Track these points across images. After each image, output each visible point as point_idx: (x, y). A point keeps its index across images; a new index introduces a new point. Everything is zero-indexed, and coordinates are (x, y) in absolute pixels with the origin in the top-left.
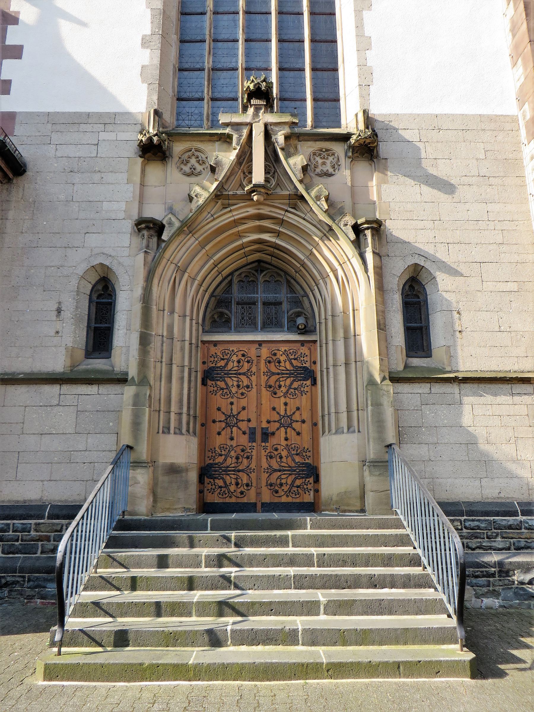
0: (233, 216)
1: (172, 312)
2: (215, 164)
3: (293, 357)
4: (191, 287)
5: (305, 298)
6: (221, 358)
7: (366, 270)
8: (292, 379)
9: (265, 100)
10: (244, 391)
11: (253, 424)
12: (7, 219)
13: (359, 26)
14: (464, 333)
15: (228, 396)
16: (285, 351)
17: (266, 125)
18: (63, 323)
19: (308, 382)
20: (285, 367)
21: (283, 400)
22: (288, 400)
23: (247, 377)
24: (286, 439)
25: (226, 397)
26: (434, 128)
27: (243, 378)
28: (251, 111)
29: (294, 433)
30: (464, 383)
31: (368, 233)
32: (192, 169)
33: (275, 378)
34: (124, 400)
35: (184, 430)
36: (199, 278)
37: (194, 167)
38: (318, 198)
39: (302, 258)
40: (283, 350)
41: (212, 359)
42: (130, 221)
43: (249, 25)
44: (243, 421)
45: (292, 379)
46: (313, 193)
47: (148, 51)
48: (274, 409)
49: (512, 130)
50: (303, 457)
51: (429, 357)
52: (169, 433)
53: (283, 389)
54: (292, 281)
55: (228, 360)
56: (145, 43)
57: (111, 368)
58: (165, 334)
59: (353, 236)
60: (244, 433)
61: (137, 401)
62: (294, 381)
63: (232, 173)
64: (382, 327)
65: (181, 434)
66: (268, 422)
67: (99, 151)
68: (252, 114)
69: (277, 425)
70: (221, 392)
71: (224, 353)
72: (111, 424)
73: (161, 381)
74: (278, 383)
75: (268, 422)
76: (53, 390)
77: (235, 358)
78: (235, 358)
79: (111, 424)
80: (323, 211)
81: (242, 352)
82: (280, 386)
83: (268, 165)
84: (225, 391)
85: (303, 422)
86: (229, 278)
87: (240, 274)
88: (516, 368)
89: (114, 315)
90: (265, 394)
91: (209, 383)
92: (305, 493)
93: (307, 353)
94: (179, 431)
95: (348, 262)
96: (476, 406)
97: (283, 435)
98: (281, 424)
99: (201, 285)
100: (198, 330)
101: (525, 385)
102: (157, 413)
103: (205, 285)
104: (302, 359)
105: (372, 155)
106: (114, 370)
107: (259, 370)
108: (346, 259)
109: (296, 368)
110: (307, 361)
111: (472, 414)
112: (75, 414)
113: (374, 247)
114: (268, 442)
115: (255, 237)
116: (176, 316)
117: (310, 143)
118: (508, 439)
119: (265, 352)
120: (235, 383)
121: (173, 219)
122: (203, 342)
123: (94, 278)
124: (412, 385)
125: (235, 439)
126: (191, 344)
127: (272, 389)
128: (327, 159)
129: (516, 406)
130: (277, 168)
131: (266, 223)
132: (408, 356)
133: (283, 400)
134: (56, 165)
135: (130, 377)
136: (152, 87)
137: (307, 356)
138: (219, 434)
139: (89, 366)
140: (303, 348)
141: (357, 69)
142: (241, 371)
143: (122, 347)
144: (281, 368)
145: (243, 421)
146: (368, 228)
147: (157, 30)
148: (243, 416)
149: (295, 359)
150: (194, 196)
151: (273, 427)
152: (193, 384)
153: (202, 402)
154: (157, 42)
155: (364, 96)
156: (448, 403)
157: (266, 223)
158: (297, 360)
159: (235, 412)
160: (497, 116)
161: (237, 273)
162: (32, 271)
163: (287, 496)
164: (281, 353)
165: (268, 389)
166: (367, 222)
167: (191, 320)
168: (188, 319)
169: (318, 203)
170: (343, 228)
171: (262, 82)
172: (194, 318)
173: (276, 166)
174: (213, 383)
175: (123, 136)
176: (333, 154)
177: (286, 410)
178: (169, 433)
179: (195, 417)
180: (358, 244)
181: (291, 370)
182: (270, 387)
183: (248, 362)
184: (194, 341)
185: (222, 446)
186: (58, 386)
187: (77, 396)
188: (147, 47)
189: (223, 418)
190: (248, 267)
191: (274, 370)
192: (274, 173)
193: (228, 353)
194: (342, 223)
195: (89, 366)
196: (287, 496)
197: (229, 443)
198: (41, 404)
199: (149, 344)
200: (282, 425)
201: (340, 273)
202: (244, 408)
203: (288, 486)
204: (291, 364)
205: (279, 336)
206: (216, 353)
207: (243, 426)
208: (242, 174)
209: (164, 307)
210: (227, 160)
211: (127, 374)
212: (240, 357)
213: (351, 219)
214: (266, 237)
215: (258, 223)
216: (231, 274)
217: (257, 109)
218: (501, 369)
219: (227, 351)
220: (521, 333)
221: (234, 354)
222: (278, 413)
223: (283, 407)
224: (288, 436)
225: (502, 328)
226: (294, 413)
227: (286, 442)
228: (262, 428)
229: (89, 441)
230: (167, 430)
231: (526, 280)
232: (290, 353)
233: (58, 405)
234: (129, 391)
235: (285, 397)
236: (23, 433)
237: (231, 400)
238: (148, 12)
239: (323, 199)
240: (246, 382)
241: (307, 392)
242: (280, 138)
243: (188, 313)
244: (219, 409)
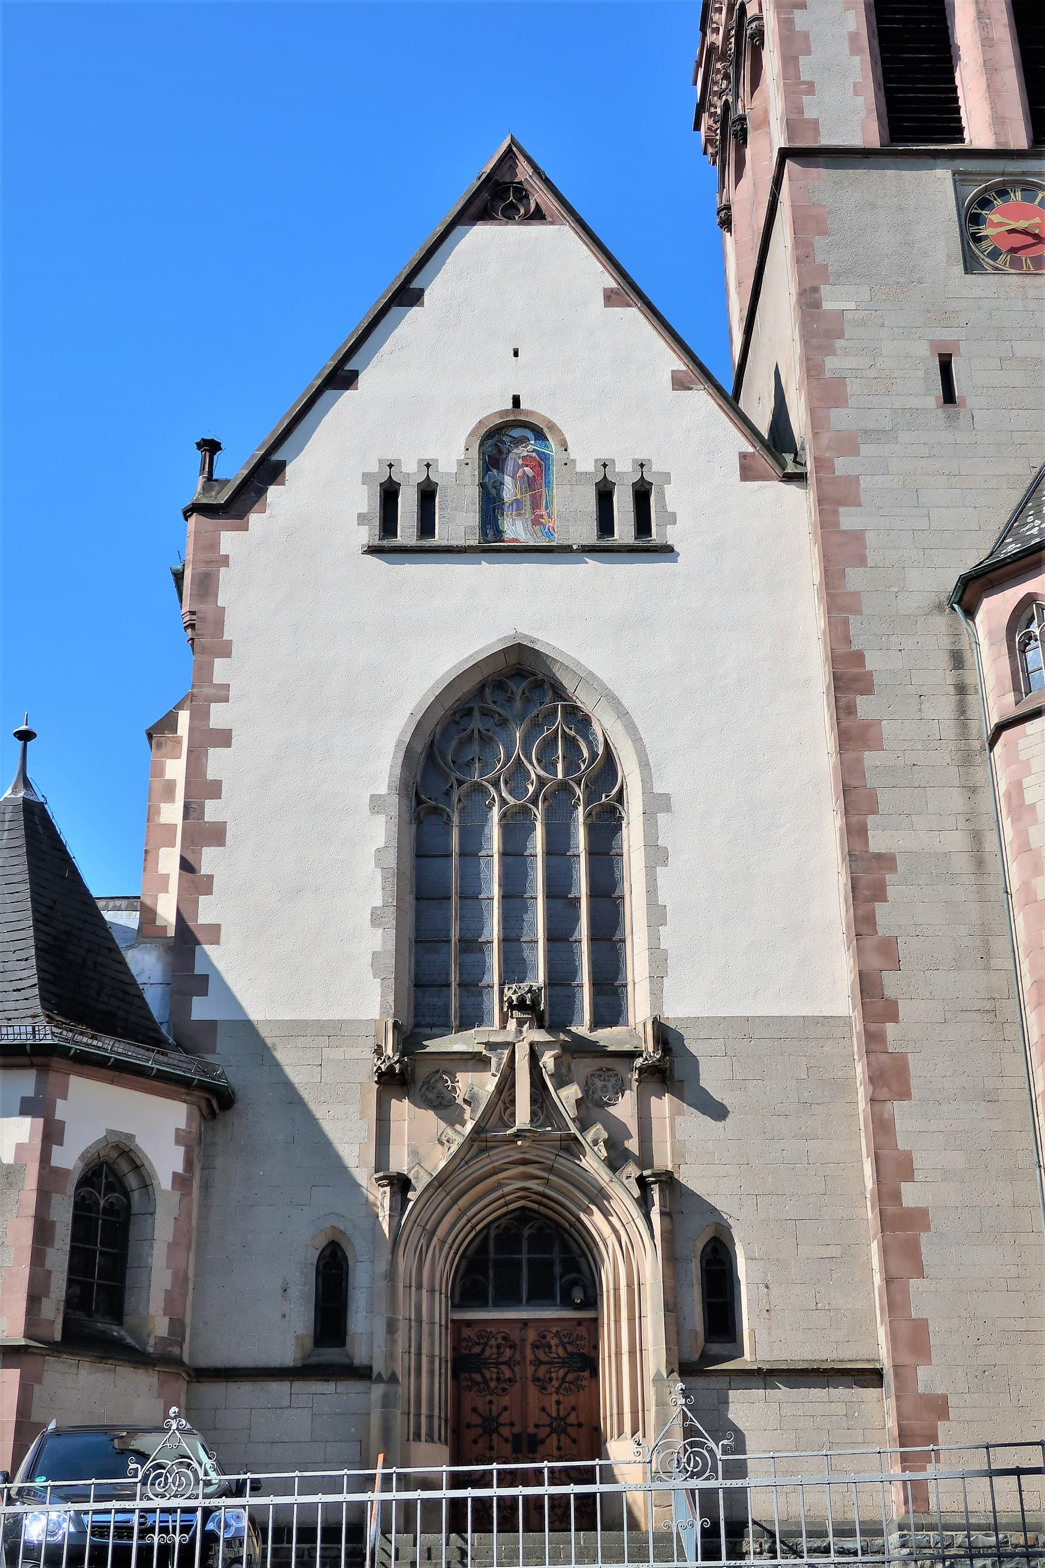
0: (492, 1162)
1: (419, 1287)
2: (471, 1098)
3: (566, 1340)
5: (583, 1260)
6: (476, 1343)
7: (653, 1237)
8: (566, 1369)
9: (530, 1012)
10: (506, 1386)
11: (516, 1430)
12: (214, 1168)
13: (652, 890)
14: (772, 1313)
15: (486, 1393)
17: (532, 1045)
18: (290, 1304)
19: (586, 1374)
20: (558, 1355)
21: (555, 1397)
22: (561, 1398)
23: (510, 1368)
25: (483, 1394)
26: (744, 1037)
27: (504, 1368)
29: (568, 1441)
30: (770, 1376)
31: (656, 1188)
32: (440, 1098)
34: (373, 1400)
36: (450, 1241)
37: (442, 1095)
40: (554, 1331)
41: (465, 1344)
42: (365, 1170)
43: (507, 917)
45: (566, 1369)
47: (380, 931)
48: (543, 1409)
49: (844, 1038)
50: (471, 1379)
51: (732, 1342)
52: (420, 1440)
53: (555, 1383)
54: (566, 1235)
55: (486, 1345)
57: (347, 1360)
58: (413, 1317)
59: (636, 1192)
60: (506, 1441)
61: (387, 1402)
62: (568, 1372)
63: (491, 1106)
64: (671, 1308)
65: (433, 1441)
66: (537, 1426)
67: (324, 1074)
68: (513, 1029)
69: (548, 1430)
70: (477, 1387)
71: (479, 1337)
72: (353, 1429)
73: (409, 1377)
74: (548, 1376)
75: (537, 1426)
76: (280, 1389)
77: (493, 1342)
79: (353, 1429)
81: (503, 1334)
82: (551, 1379)
83: (535, 1092)
84: (482, 1386)
85: (580, 1425)
86: (484, 1233)
87: (498, 1227)
88: (834, 1356)
90: (532, 1390)
91: (463, 1375)
92: (583, 1517)
93: (584, 1333)
94: (430, 1438)
95: (632, 1222)
96: (784, 1404)
97: (555, 1443)
98: (552, 1429)
99: (451, 1248)
100: (447, 1306)
101: (845, 1377)
102: (407, 1416)
103: (455, 1247)
104: (578, 1342)
105: (664, 1077)
106: (353, 1363)
107: (524, 1358)
108: (631, 1219)
109: (571, 1355)
110: (584, 1346)
111: (778, 1414)
112: (310, 1418)
113: (662, 1205)
114: (536, 1452)
116: (424, 1291)
119: (531, 1335)
120: (494, 1376)
121: (422, 1173)
122: (453, 1321)
123: (322, 1243)
124: (707, 1379)
125: (496, 1448)
126: (440, 1326)
127: (540, 1383)
128: (609, 1081)
129: (832, 1404)
130: (545, 1098)
132: (708, 1340)
133: (555, 1397)
134: (271, 1094)
136: (386, 982)
137: (585, 1338)
138: (475, 1442)
139: (321, 1358)
140: (579, 1328)
142: (501, 1360)
143: (362, 1334)
144: (553, 1355)
146: (655, 1183)
147: (390, 900)
148: (505, 1418)
149: (569, 1343)
150: (445, 1142)
151: (543, 1432)
153: (453, 1399)
154: (391, 920)
155: (656, 994)
156: (751, 1401)
158: (572, 1344)
160: (825, 1017)
162: (249, 1237)
163: (491, 1332)
164: (552, 1335)
165: (536, 1383)
166: (654, 1175)
167: (441, 1294)
168: (437, 1294)
169: (596, 1148)
170: (626, 1182)
171: (527, 993)
172: (443, 1292)
173: (543, 1095)
174: (467, 1375)
175: (354, 1053)
176: (616, 1075)
177: (558, 1411)
178: (420, 1440)
179: (446, 1421)
180: (644, 1203)
181: (564, 1358)
182: (538, 1380)
183: (510, 1347)
184: (443, 1323)
185: (479, 1458)
186: (288, 1384)
187: (311, 1396)
188: (379, 926)
190: (510, 1216)
191: (543, 1357)
192: (542, 1103)
193: (485, 1336)
194: (624, 1176)
195: (321, 1358)
196: (491, 1332)
197: (561, 1398)
198: (269, 1406)
199: (396, 1333)
200: (553, 1431)
202: (505, 1409)
203: (562, 1510)
204: (565, 1349)
205: (549, 1313)
206: (469, 1336)
207: (506, 1432)
208: (502, 1105)
209: (410, 1282)
210: (484, 1092)
212: (500, 1340)
213: (636, 1170)
215: (521, 1169)
216: (487, 1227)
217: (521, 1023)
218: (816, 1358)
219: (483, 1334)
220: (842, 1312)
221: (493, 1337)
222: (548, 1415)
223: (554, 1407)
224: (562, 1444)
225: (820, 1305)
226: (569, 1414)
227: (559, 1453)
228: (530, 1435)
229: (327, 1450)
230: (418, 1437)
232: (564, 1335)
233: (290, 1407)
234: (377, 1391)
235: (557, 1393)
236: (250, 1442)
237: (489, 1398)
239: (602, 1143)
240: (508, 1374)
241: (585, 1386)
242: (548, 1060)
243: (437, 1288)
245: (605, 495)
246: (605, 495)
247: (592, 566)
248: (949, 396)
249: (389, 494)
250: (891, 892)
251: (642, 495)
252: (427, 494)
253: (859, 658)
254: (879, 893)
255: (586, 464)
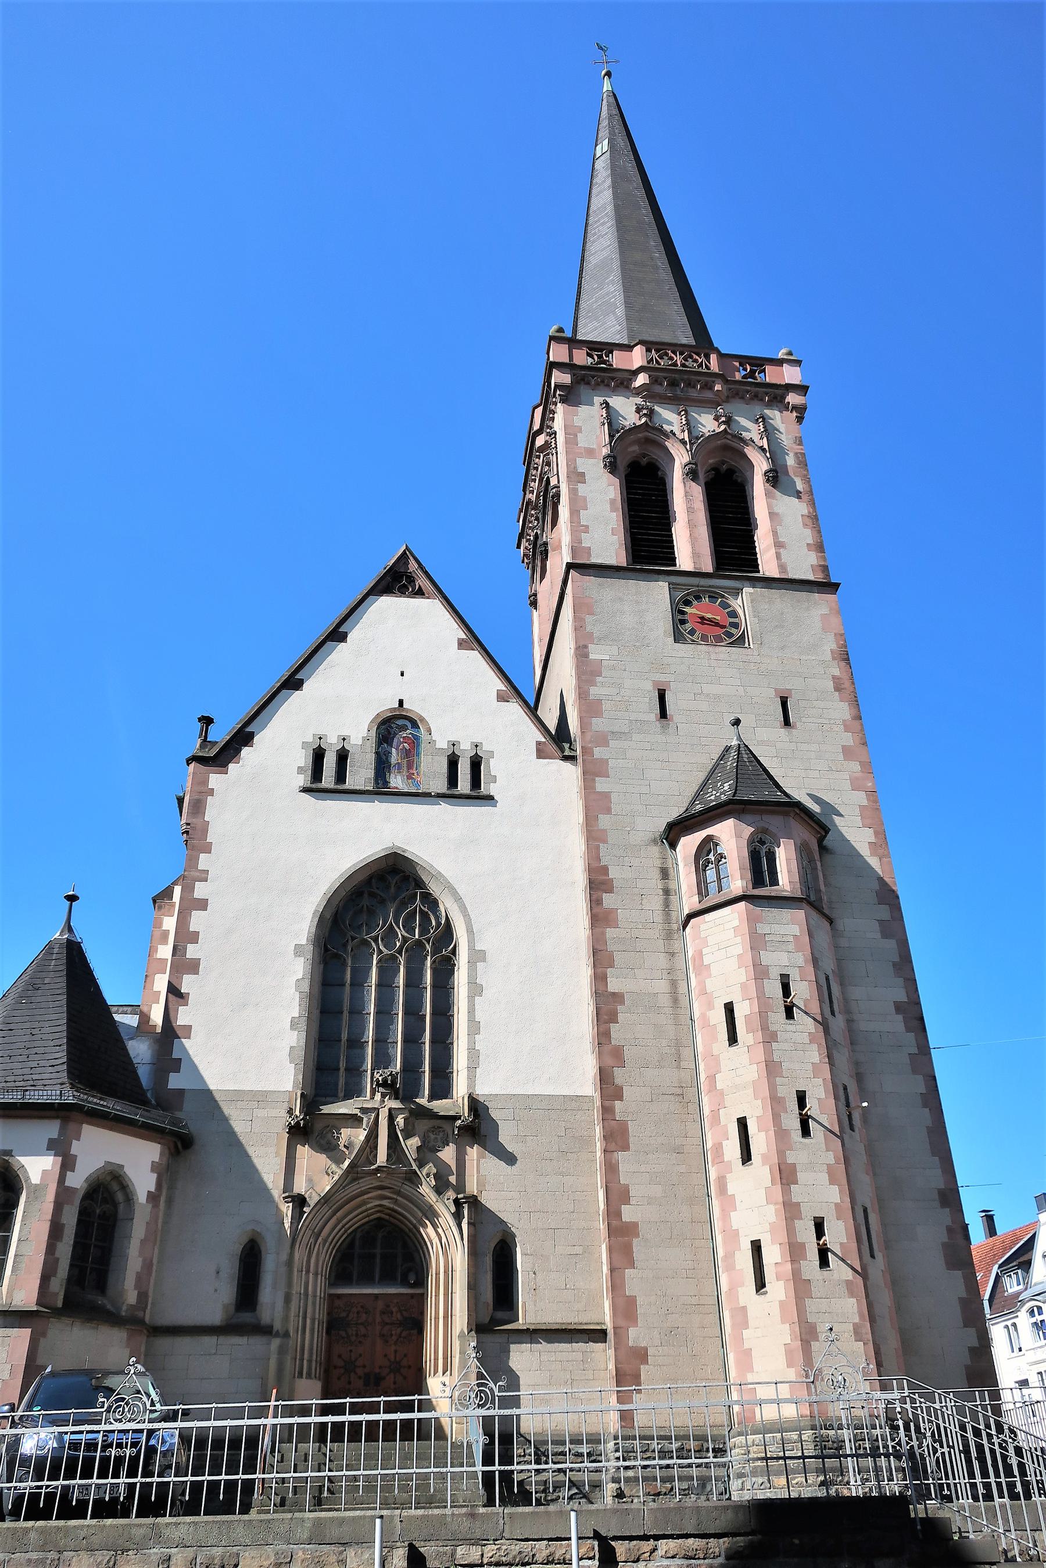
1: (308, 1271)
4: (323, 1248)
13: (471, 1011)
14: (537, 1291)
16: (397, 1303)
17: (390, 1110)
19: (415, 1332)
21: (393, 1348)
24: (395, 1383)
28: (378, 1096)
31: (466, 1206)
33: (388, 1327)
35: (313, 1376)
38: (428, 1175)
39: (415, 1222)
44: (359, 1367)
46: (425, 1172)
48: (386, 1356)
56: (293, 1025)
59: (453, 1209)
60: (360, 1378)
61: (282, 1351)
63: (362, 1150)
72: (257, 1370)
75: (380, 1367)
78: (355, 1310)
80: (548, 358)
82: (392, 1335)
84: (346, 1339)
88: (576, 1321)
89: (259, 1274)
115: (378, 1203)
117: (425, 1121)
118: (566, 1380)
119: (380, 1305)
120: (354, 1333)
121: (314, 1194)
123: (245, 1240)
128: (439, 1135)
131: (386, 1193)
135: (275, 1329)
136: (298, 1067)
138: (339, 1379)
141: (466, 1051)
145: (359, 1367)
146: (465, 1203)
152: (320, 1334)
154: (303, 1026)
155: (472, 1079)
157: (386, 1193)
159: (353, 1359)
161: (360, 1230)
168: (319, 1276)
169: (428, 1179)
170: (446, 1202)
175: (274, 1113)
176: (444, 1131)
179: (320, 1364)
180: (458, 1216)
182: (383, 1335)
183: (366, 1313)
188: (295, 1029)
189: (342, 1364)
191: (387, 1320)
201: (444, 1239)
202: (360, 1355)
211: (272, 1327)
214: (385, 1202)
215: (380, 1192)
231: (590, 1244)
234: (276, 1342)
237: (350, 1348)
238: (297, 995)
244: (340, 1356)
245: (453, 763)
246: (453, 763)
247: (444, 809)
248: (663, 714)
249: (319, 755)
250: (621, 1017)
251: (476, 764)
252: (343, 757)
253: (605, 870)
254: (613, 1018)
255: (442, 744)
